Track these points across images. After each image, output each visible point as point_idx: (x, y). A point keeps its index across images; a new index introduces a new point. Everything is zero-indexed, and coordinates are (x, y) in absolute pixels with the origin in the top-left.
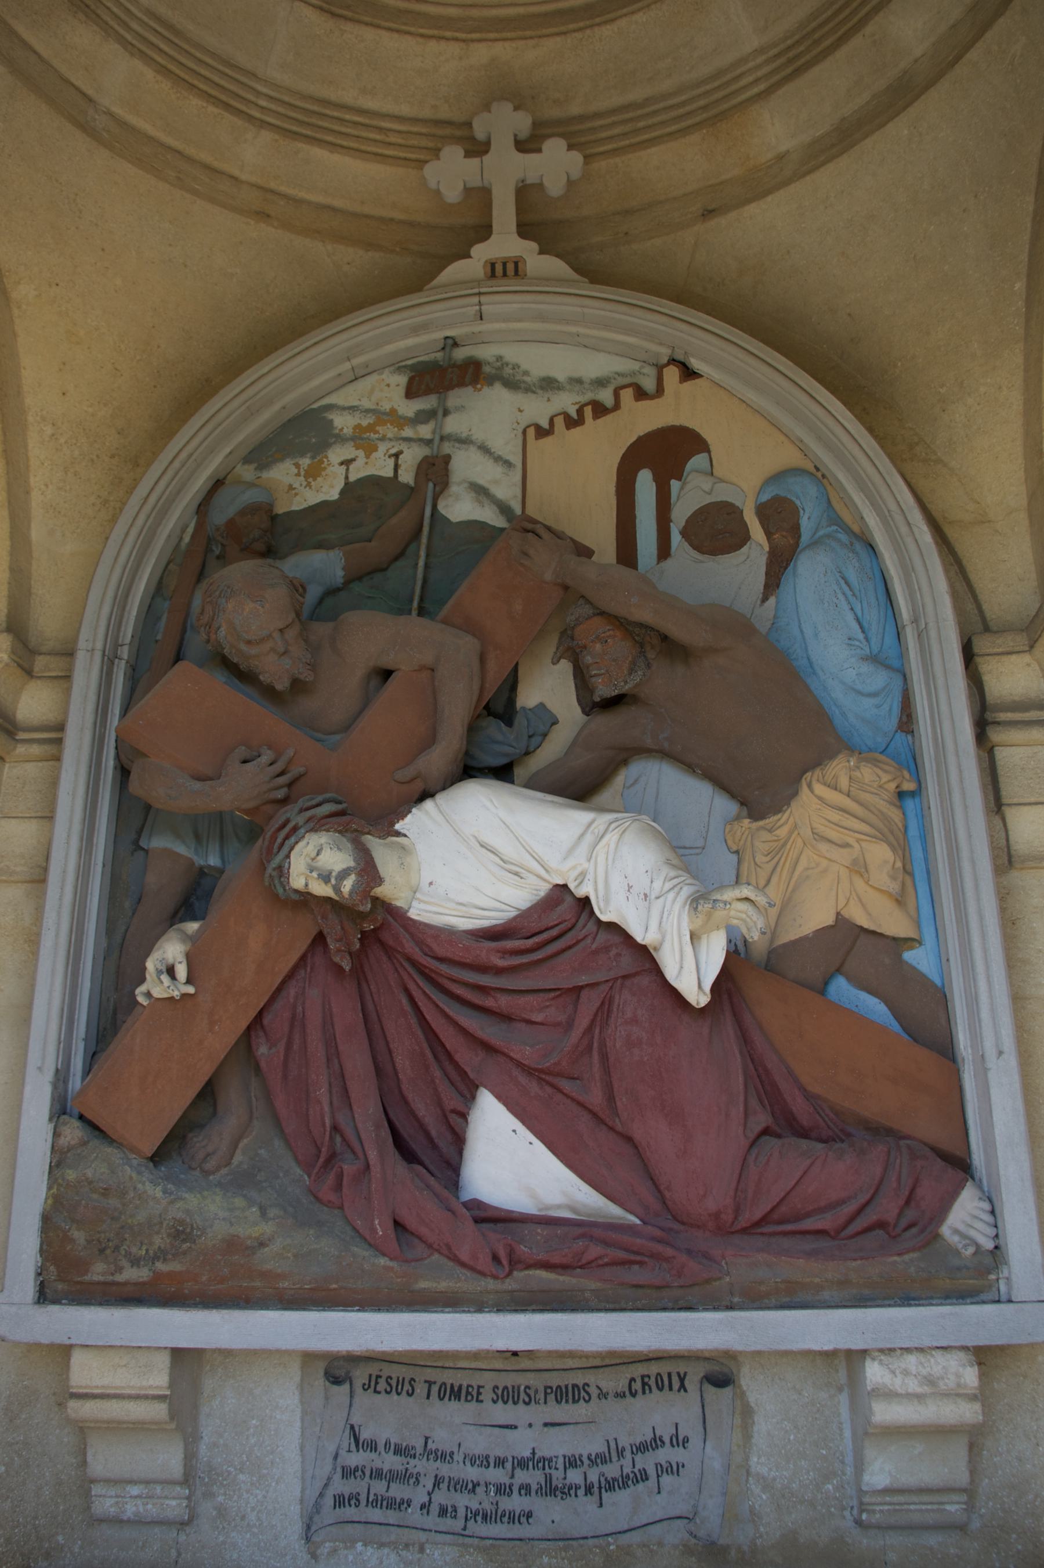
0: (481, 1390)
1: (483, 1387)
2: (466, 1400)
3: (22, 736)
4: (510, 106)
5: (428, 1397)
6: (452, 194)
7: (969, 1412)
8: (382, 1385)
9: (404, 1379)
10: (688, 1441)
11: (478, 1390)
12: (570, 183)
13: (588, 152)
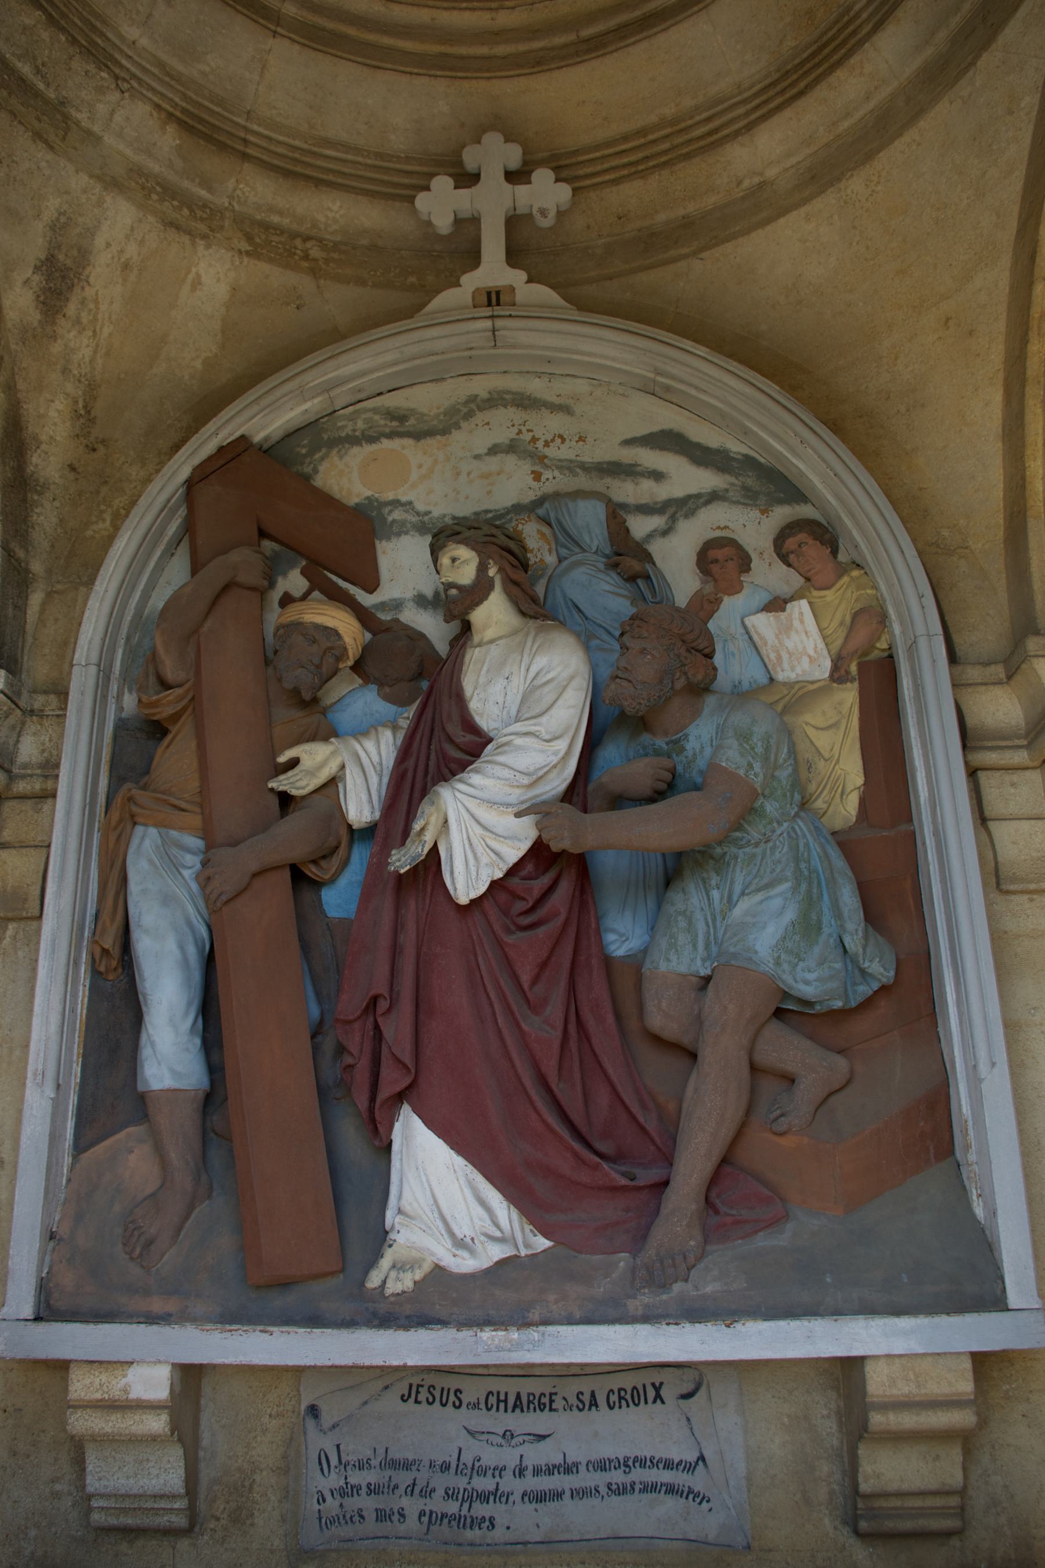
0: (554, 1397)
4: (449, 182)
6: (443, 223)
7: (963, 1418)
8: (423, 1395)
9: (449, 1390)
10: (403, 1396)
11: (551, 1397)
12: (560, 214)
13: (577, 185)
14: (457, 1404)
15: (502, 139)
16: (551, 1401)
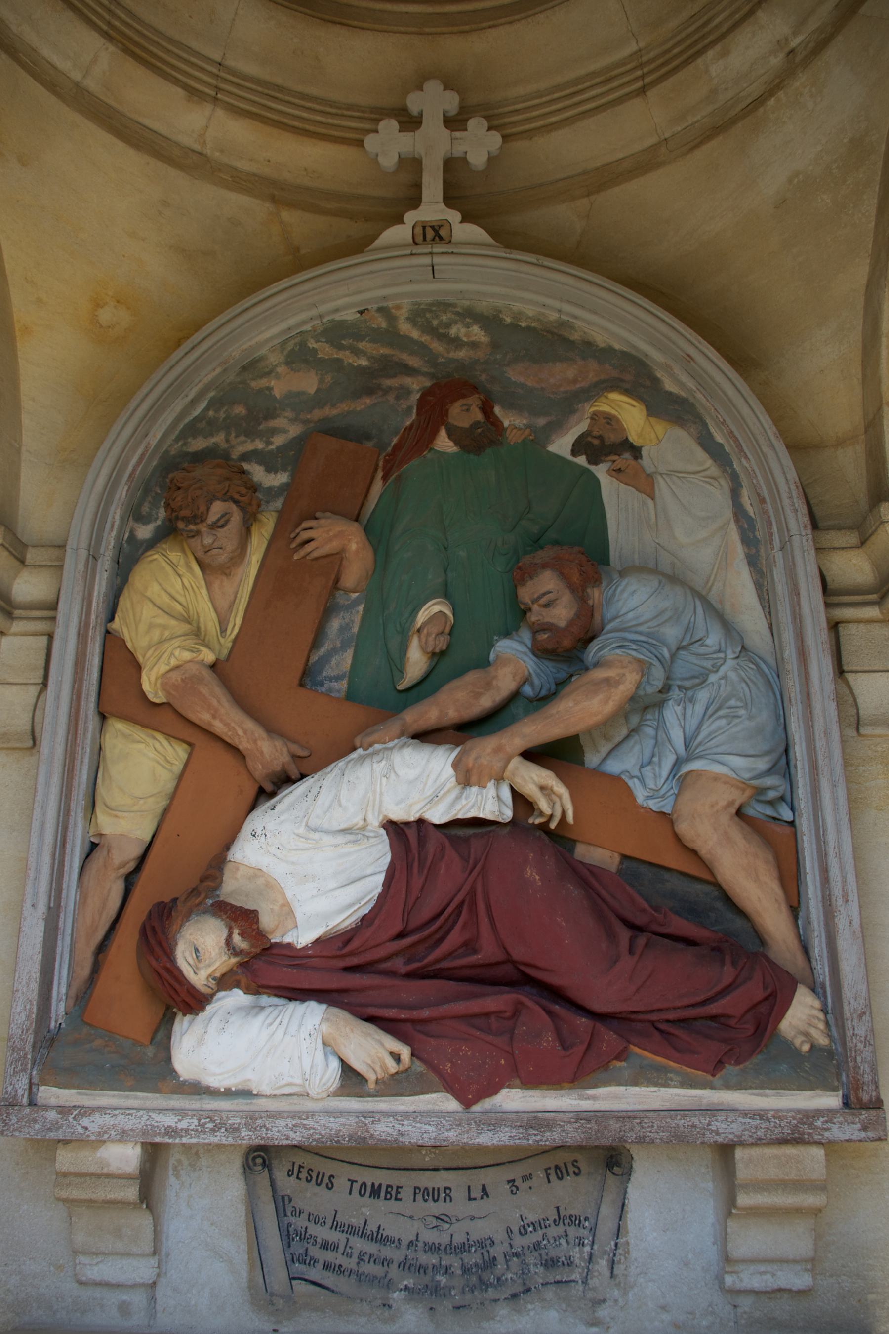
0: (399, 1190)
1: (401, 1187)
2: (386, 1198)
3: (17, 613)
4: (394, 124)
5: (350, 1193)
6: (389, 162)
11: (397, 1190)
13: (508, 131)
14: (330, 1186)
15: (442, 87)
16: (398, 1192)
